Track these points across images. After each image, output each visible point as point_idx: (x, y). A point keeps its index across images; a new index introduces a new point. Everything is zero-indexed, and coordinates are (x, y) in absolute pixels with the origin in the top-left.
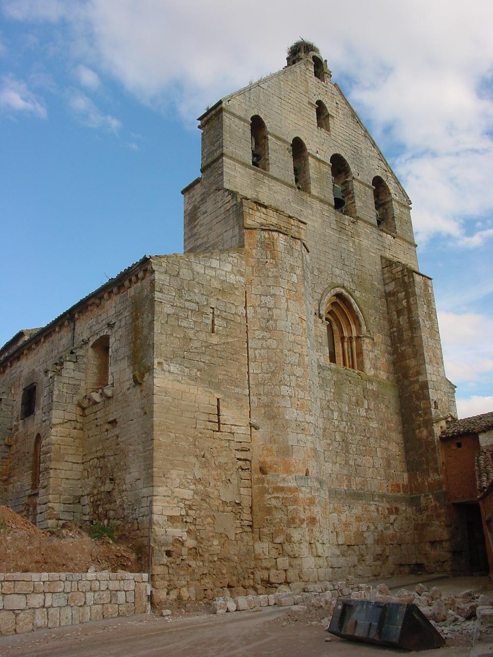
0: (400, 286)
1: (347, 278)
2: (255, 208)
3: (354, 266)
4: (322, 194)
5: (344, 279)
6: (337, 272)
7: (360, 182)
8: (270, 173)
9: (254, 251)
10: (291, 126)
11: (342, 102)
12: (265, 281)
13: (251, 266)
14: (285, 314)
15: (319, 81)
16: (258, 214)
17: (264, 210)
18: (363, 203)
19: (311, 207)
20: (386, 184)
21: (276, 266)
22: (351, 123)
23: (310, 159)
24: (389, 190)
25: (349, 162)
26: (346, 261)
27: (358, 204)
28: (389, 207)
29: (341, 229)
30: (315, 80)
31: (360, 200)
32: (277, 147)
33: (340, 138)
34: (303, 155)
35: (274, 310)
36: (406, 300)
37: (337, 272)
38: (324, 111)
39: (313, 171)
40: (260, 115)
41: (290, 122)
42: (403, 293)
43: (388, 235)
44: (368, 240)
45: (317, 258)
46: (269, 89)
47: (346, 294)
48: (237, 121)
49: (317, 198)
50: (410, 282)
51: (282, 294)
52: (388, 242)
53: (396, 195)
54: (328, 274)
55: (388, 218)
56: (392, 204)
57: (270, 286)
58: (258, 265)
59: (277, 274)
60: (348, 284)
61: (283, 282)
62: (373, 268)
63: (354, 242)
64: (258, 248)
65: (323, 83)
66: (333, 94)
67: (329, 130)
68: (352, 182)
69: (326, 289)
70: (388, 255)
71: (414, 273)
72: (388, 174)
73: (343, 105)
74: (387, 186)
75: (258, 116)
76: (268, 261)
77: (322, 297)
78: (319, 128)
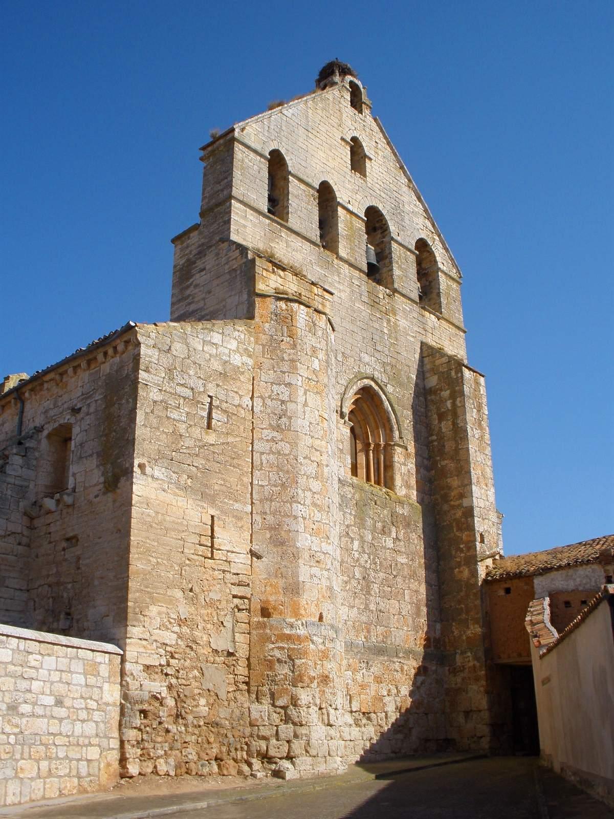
3: (387, 353)
4: (351, 256)
5: (371, 365)
7: (400, 244)
8: (290, 225)
9: (267, 325)
11: (384, 142)
15: (356, 112)
16: (273, 276)
17: (281, 273)
20: (431, 249)
21: (294, 346)
23: (340, 209)
24: (435, 257)
25: (387, 217)
27: (397, 272)
29: (374, 303)
31: (400, 267)
32: (300, 192)
33: (378, 186)
34: (330, 204)
36: (451, 401)
37: (367, 358)
41: (317, 161)
42: (448, 392)
44: (407, 320)
46: (294, 118)
47: (376, 388)
48: (252, 155)
50: (457, 377)
51: (299, 383)
52: (430, 324)
54: (355, 360)
57: (284, 373)
59: (295, 357)
61: (301, 368)
63: (389, 321)
64: (272, 322)
67: (365, 176)
68: (390, 243)
72: (435, 237)
73: (383, 145)
74: (433, 252)
76: (285, 339)
77: (345, 390)
78: (353, 171)
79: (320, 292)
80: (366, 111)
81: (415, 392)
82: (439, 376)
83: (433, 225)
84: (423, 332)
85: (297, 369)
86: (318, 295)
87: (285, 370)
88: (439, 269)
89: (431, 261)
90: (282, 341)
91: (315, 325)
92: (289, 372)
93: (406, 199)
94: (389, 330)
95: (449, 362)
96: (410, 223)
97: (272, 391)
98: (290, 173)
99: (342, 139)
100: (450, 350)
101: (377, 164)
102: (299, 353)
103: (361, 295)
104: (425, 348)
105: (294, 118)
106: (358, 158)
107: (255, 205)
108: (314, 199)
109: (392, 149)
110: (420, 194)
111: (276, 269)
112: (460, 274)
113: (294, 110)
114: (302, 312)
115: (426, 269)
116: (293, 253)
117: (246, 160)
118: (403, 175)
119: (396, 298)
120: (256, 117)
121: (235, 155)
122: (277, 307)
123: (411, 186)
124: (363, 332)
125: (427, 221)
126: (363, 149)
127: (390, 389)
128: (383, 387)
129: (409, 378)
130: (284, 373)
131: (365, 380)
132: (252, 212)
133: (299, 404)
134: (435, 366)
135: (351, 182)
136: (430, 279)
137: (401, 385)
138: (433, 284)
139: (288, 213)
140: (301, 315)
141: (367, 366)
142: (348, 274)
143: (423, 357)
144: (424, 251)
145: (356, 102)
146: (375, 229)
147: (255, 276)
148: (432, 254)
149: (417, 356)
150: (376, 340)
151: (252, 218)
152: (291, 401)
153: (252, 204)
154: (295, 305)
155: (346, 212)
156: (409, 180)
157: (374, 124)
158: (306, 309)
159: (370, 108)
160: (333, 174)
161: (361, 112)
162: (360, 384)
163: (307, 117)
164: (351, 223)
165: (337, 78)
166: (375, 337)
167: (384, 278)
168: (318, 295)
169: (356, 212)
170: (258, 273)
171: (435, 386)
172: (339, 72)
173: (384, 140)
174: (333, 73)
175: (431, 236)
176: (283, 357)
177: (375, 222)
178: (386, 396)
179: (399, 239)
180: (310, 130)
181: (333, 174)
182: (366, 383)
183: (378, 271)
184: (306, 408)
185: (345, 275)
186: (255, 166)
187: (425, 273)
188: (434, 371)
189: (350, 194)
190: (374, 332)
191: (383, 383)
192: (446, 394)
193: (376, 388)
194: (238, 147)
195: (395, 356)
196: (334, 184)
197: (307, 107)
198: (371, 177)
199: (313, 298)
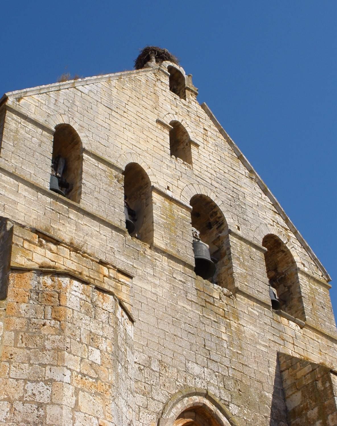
0: (310, 398)
1: (214, 381)
2: (36, 241)
3: (227, 363)
4: (173, 248)
5: (204, 378)
6: (197, 370)
7: (241, 238)
8: (81, 205)
9: (23, 306)
10: (124, 147)
11: (214, 130)
12: (35, 356)
13: (14, 330)
14: (71, 416)
15: (178, 97)
16: (39, 250)
17: (53, 247)
18: (246, 270)
19: (152, 264)
20: (286, 248)
21: (61, 331)
22: (227, 158)
23: (154, 195)
24: (291, 256)
25: (222, 208)
26: (213, 353)
27: (237, 269)
28: (293, 283)
29: (206, 304)
30: (170, 95)
31: (242, 265)
32: (98, 172)
33: (209, 175)
34: (144, 191)
35: (48, 407)
36: (321, 421)
37: (197, 370)
38: (184, 137)
39: (159, 213)
40: (71, 124)
41: (124, 142)
42: (316, 410)
43: (290, 321)
44: (255, 326)
45: (159, 343)
46: (92, 95)
47: (213, 407)
48: (30, 126)
49: (163, 252)
50: (325, 388)
51: (67, 379)
52: (289, 332)
53: (304, 265)
54: (178, 371)
55: (292, 299)
56: (298, 278)
57: (44, 366)
58: (28, 329)
59: (61, 345)
60: (217, 391)
61: (71, 359)
62: (264, 374)
63: (228, 326)
64: (31, 302)
65: (183, 100)
66: (199, 117)
67: (191, 162)
68: (228, 237)
69: (172, 396)
70: (290, 351)
71: (332, 374)
72: (289, 234)
73: (215, 133)
74: (288, 250)
75: (69, 125)
76: (48, 322)
77: (164, 408)
78: (173, 156)
79: (113, 273)
80: (191, 97)
81: (272, 414)
82: (302, 391)
83: (286, 221)
84: (281, 342)
85: (64, 360)
86: (109, 277)
87: (45, 361)
88: (298, 269)
89: (288, 263)
90: (44, 325)
91: (95, 306)
92: (52, 365)
93: (248, 191)
94: (229, 337)
95: (313, 370)
96: (254, 214)
97: (26, 391)
98: (84, 150)
99: (158, 121)
100: (316, 358)
101: (207, 152)
102: (68, 340)
103: (186, 293)
104: (282, 360)
105: (92, 95)
106: (179, 143)
107: (32, 180)
108: (118, 181)
109: (226, 137)
110: (266, 186)
111: (44, 242)
112: (327, 276)
113: (94, 88)
114: (76, 289)
115: (283, 273)
116: (86, 237)
117: (22, 131)
118: (242, 165)
119: (238, 299)
120: (38, 87)
121: (5, 125)
122: (39, 283)
123: (254, 177)
124: (191, 336)
125: (277, 216)
126: (188, 136)
127: (233, 409)
128: (224, 407)
129: (261, 396)
130: (44, 366)
131: (195, 397)
132: (26, 187)
133: (64, 407)
134: (297, 379)
135: (170, 167)
136: (289, 283)
137: (249, 404)
138: (292, 288)
139: (80, 194)
140: (73, 293)
141: (197, 379)
142: (167, 267)
143: (281, 372)
144: (278, 252)
145: (177, 85)
146: (210, 226)
147: (11, 247)
148: (287, 253)
149: (273, 370)
150: (210, 347)
151: (26, 194)
152: (53, 404)
153: (27, 178)
154: (66, 281)
155: (163, 198)
156: (251, 171)
157: (201, 112)
158: (82, 286)
159: (196, 94)
160: (145, 157)
161: (184, 98)
162: (188, 402)
163: (110, 95)
164: (171, 210)
165: (153, 63)
166: (208, 343)
167: (223, 279)
168: (109, 277)
169: (178, 198)
170: (17, 245)
171: (299, 406)
172: (156, 58)
173: (216, 129)
174: (149, 59)
175: (284, 232)
176: (44, 347)
177: (205, 214)
178: (228, 418)
179: (239, 233)
180: (114, 109)
181: (145, 157)
182: (197, 401)
183: (210, 268)
184: (77, 413)
185: (162, 268)
186: (34, 139)
187: (282, 278)
188: (296, 386)
189: (169, 180)
190: (207, 338)
191: (222, 402)
192: (313, 413)
193: (213, 407)
194: (10, 117)
195: (241, 368)
196: (147, 167)
197: (110, 86)
198: (199, 164)
199: (101, 280)
